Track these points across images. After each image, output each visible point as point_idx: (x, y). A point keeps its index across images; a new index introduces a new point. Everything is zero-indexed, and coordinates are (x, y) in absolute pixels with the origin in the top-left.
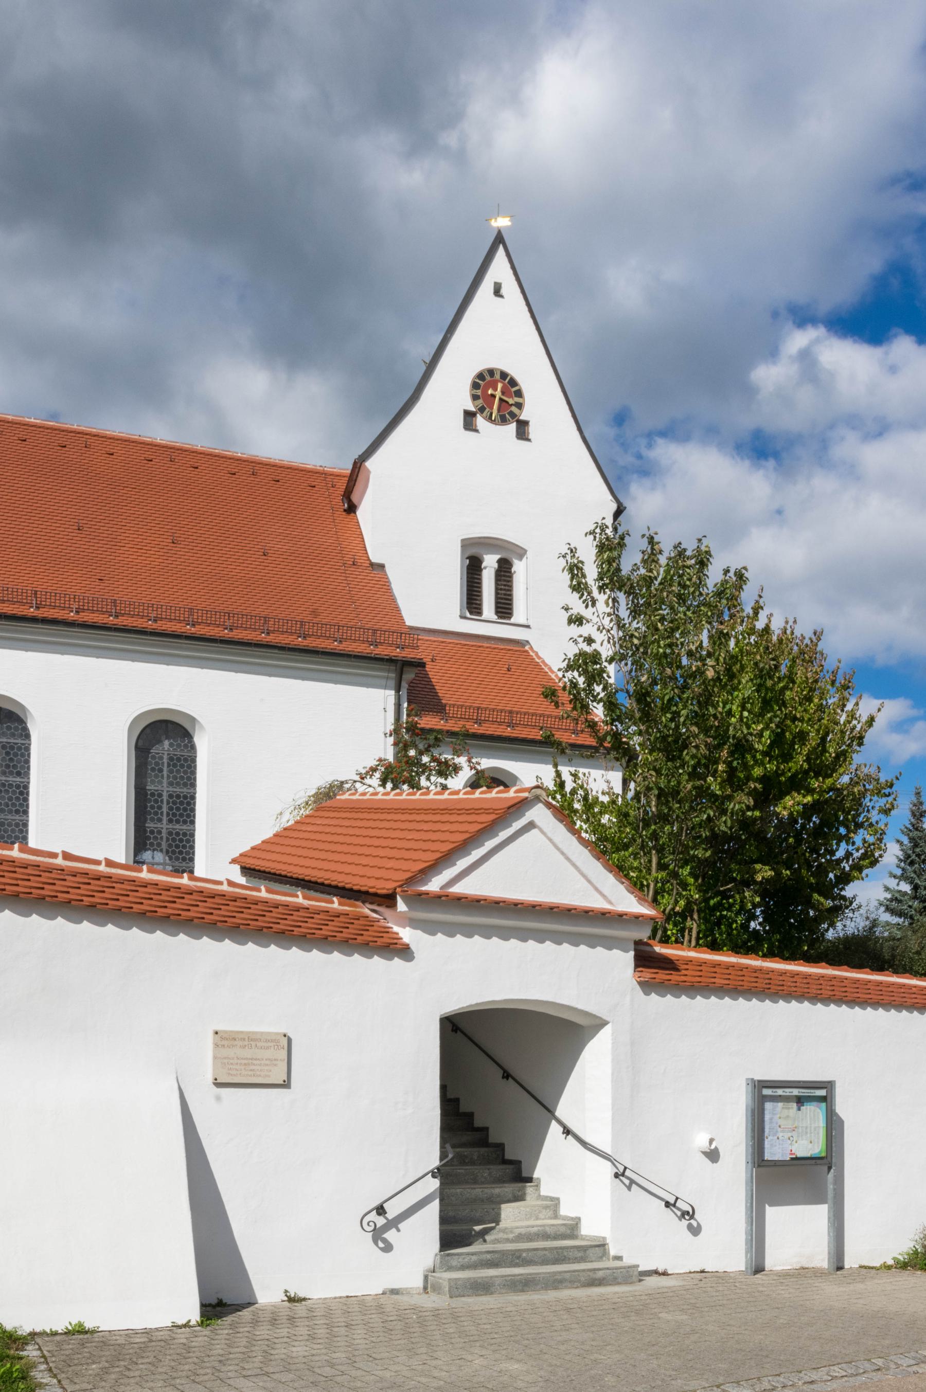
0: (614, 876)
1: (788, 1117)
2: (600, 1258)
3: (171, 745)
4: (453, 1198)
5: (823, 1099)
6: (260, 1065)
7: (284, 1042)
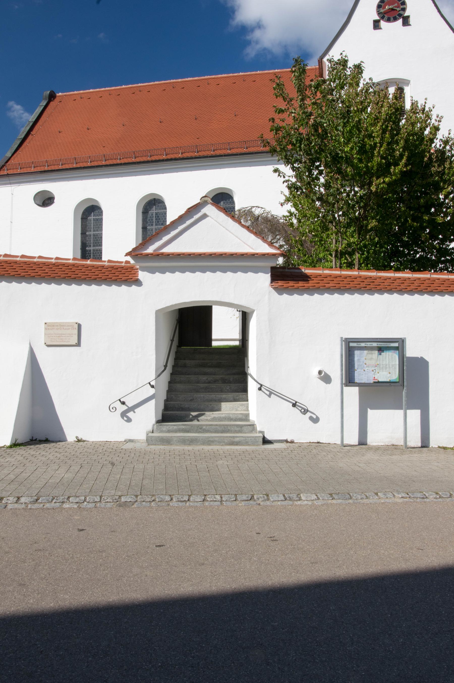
1: (372, 358)
2: (251, 432)
3: (224, 203)
4: (199, 399)
5: (396, 348)
6: (65, 337)
7: (76, 326)
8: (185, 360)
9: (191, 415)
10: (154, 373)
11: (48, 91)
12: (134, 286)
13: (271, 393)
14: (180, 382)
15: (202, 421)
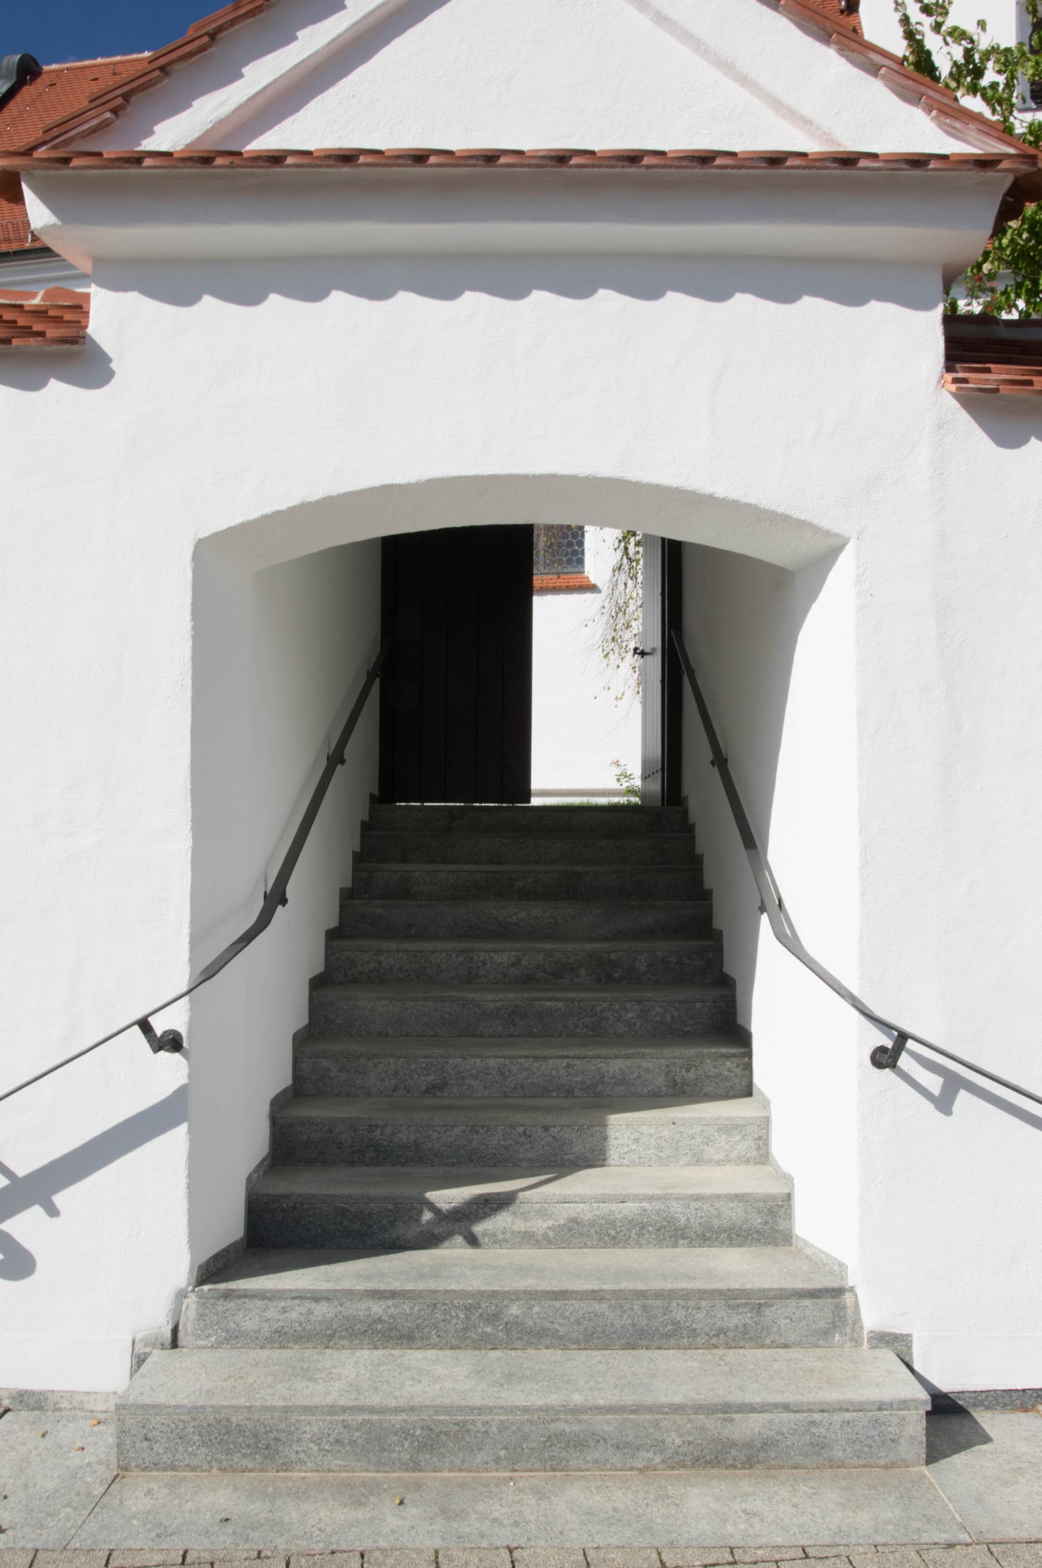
0: (841, 51)
8: (404, 860)
9: (432, 1207)
10: (185, 954)
11: (15, 53)
12: (56, 387)
13: (953, 1084)
14: (377, 979)
15: (498, 1241)
